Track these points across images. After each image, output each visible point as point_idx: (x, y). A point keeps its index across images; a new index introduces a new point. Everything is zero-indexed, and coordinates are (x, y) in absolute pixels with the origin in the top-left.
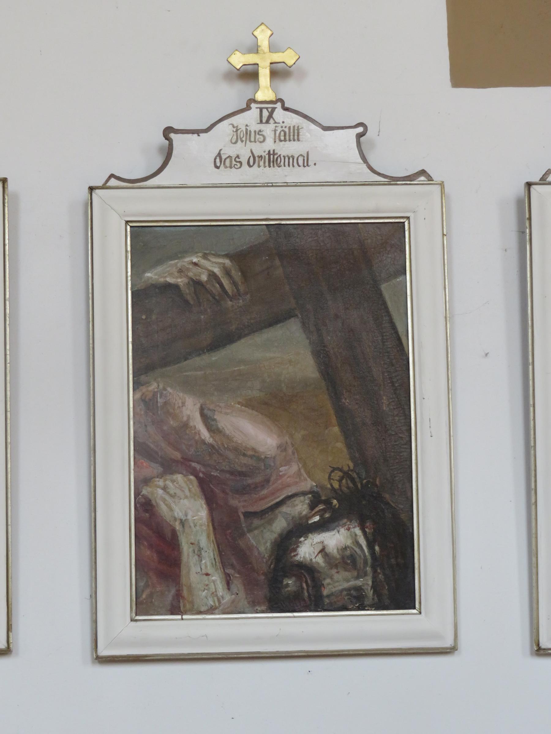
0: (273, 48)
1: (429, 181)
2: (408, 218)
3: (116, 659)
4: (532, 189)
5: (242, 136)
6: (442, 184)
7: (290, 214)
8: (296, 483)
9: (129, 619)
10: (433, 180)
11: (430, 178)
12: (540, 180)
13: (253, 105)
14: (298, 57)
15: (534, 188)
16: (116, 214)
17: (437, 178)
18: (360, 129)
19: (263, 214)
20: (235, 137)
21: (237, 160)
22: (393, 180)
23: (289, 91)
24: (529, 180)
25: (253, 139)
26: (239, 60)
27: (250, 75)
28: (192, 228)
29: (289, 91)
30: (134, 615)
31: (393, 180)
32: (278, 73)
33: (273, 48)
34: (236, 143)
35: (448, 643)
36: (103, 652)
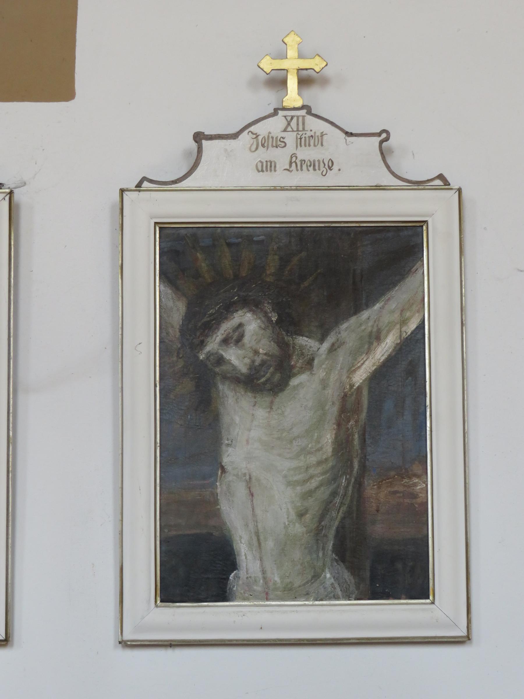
0: (283, 56)
1: (445, 185)
2: (425, 222)
3: (173, 643)
4: (124, 196)
5: (263, 142)
6: (460, 190)
7: (192, 217)
8: (338, 486)
9: (432, 606)
10: (449, 185)
11: (446, 183)
12: (136, 187)
13: (281, 113)
14: (325, 64)
15: (127, 196)
16: (145, 215)
17: (455, 184)
18: (384, 135)
19: (279, 216)
20: (255, 143)
21: (282, 140)
22: (418, 185)
23: (323, 100)
24: (124, 186)
25: (274, 145)
26: (268, 64)
27: (278, 82)
28: (269, 229)
29: (323, 100)
30: (428, 601)
31: (418, 185)
32: (305, 81)
33: (301, 56)
34: (257, 149)
35: (463, 632)
36: (128, 636)
